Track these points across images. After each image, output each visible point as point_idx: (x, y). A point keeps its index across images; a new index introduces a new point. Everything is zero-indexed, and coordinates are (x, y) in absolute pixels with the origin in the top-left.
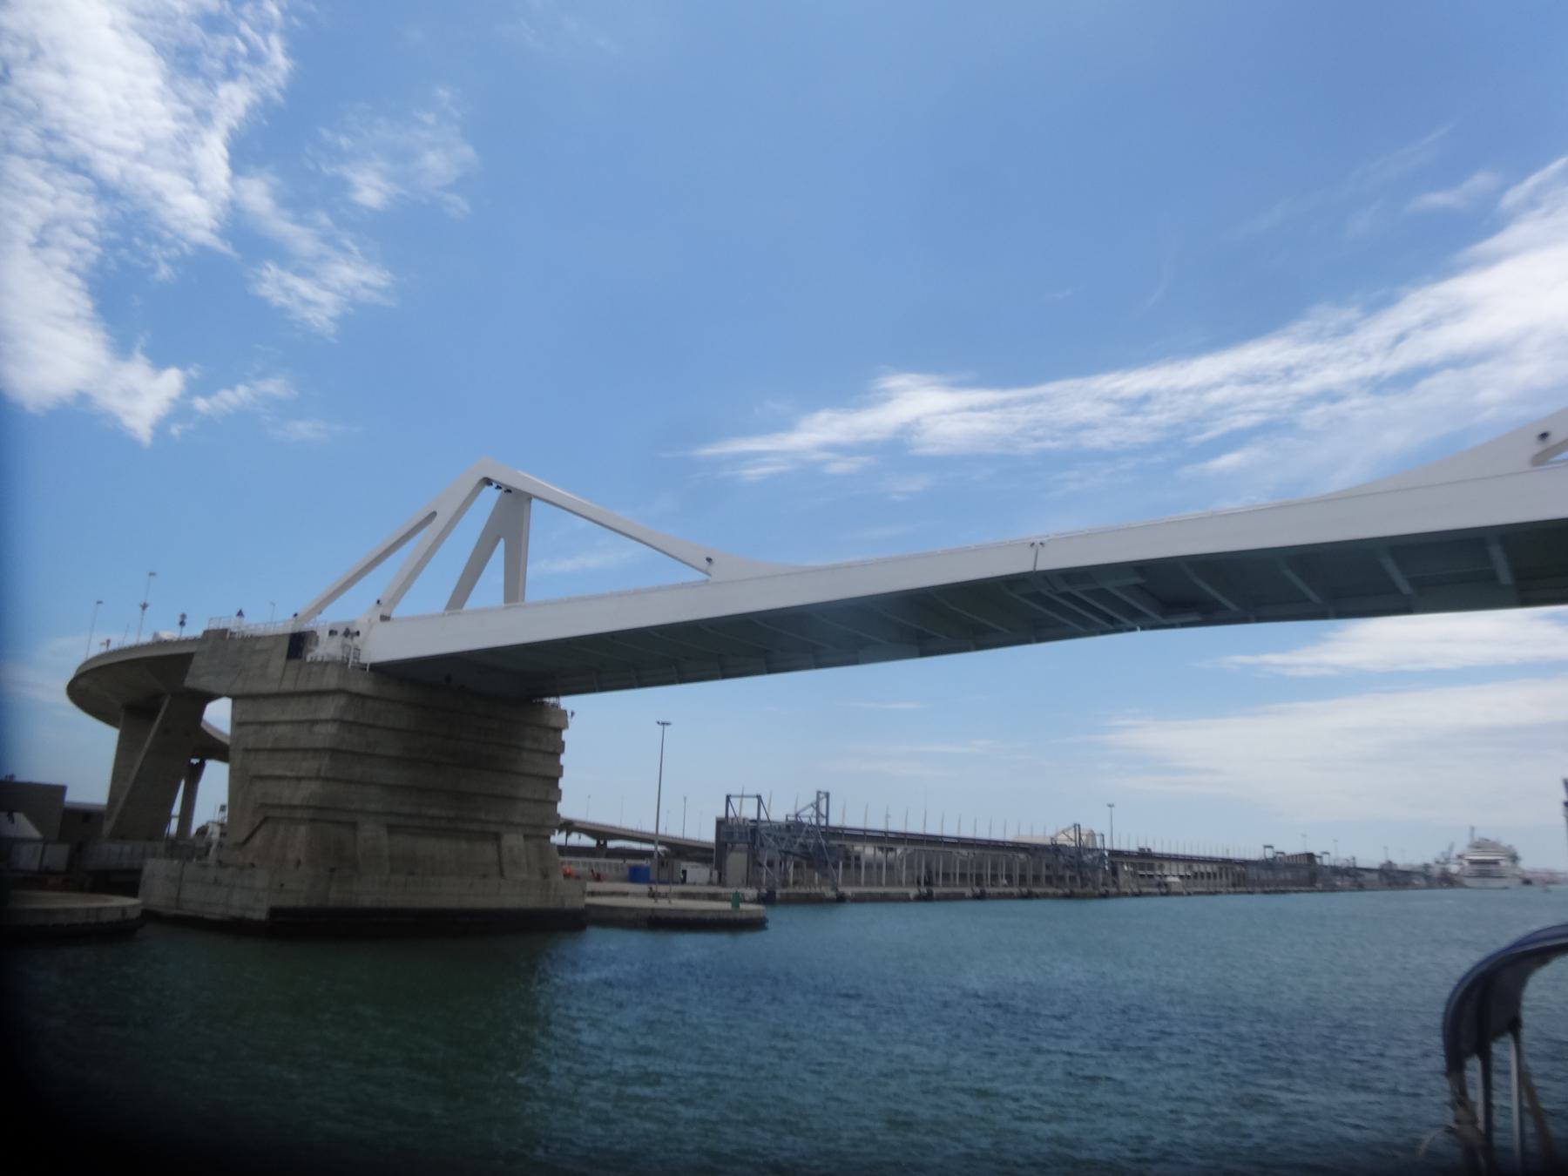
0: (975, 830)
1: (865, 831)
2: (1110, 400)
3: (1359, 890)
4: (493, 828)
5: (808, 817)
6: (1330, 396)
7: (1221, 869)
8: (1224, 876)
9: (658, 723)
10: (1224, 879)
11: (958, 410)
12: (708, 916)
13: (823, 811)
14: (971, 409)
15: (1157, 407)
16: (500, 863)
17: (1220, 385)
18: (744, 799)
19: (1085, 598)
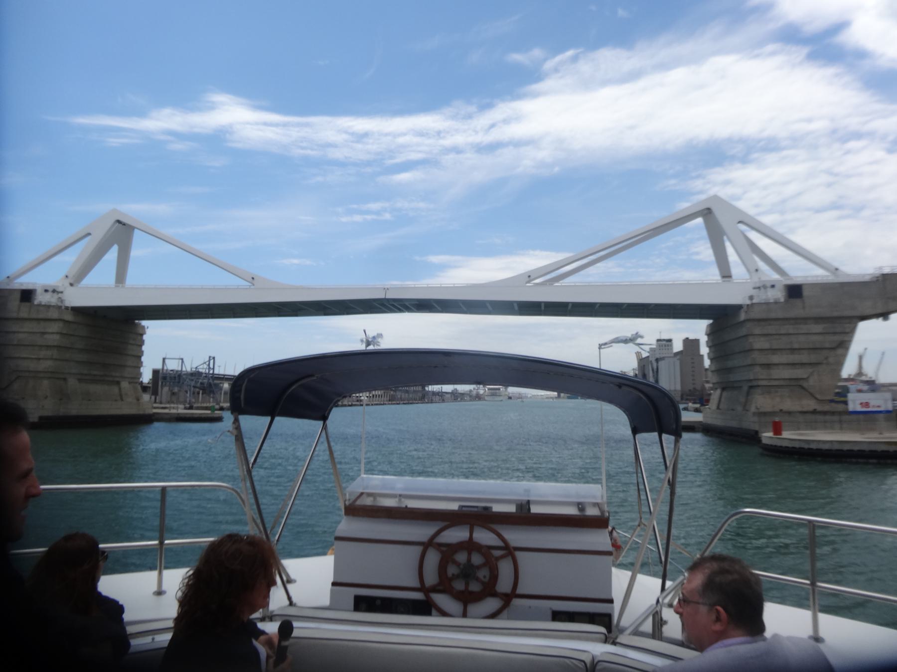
0: (225, 370)
1: (224, 375)
2: (346, 132)
3: (442, 402)
4: (117, 379)
5: (203, 369)
6: (456, 150)
7: (384, 393)
8: (386, 396)
10: (385, 398)
11: (257, 124)
12: (188, 416)
13: (211, 366)
14: (266, 124)
15: (371, 141)
16: (121, 396)
17: (404, 134)
19: (399, 307)
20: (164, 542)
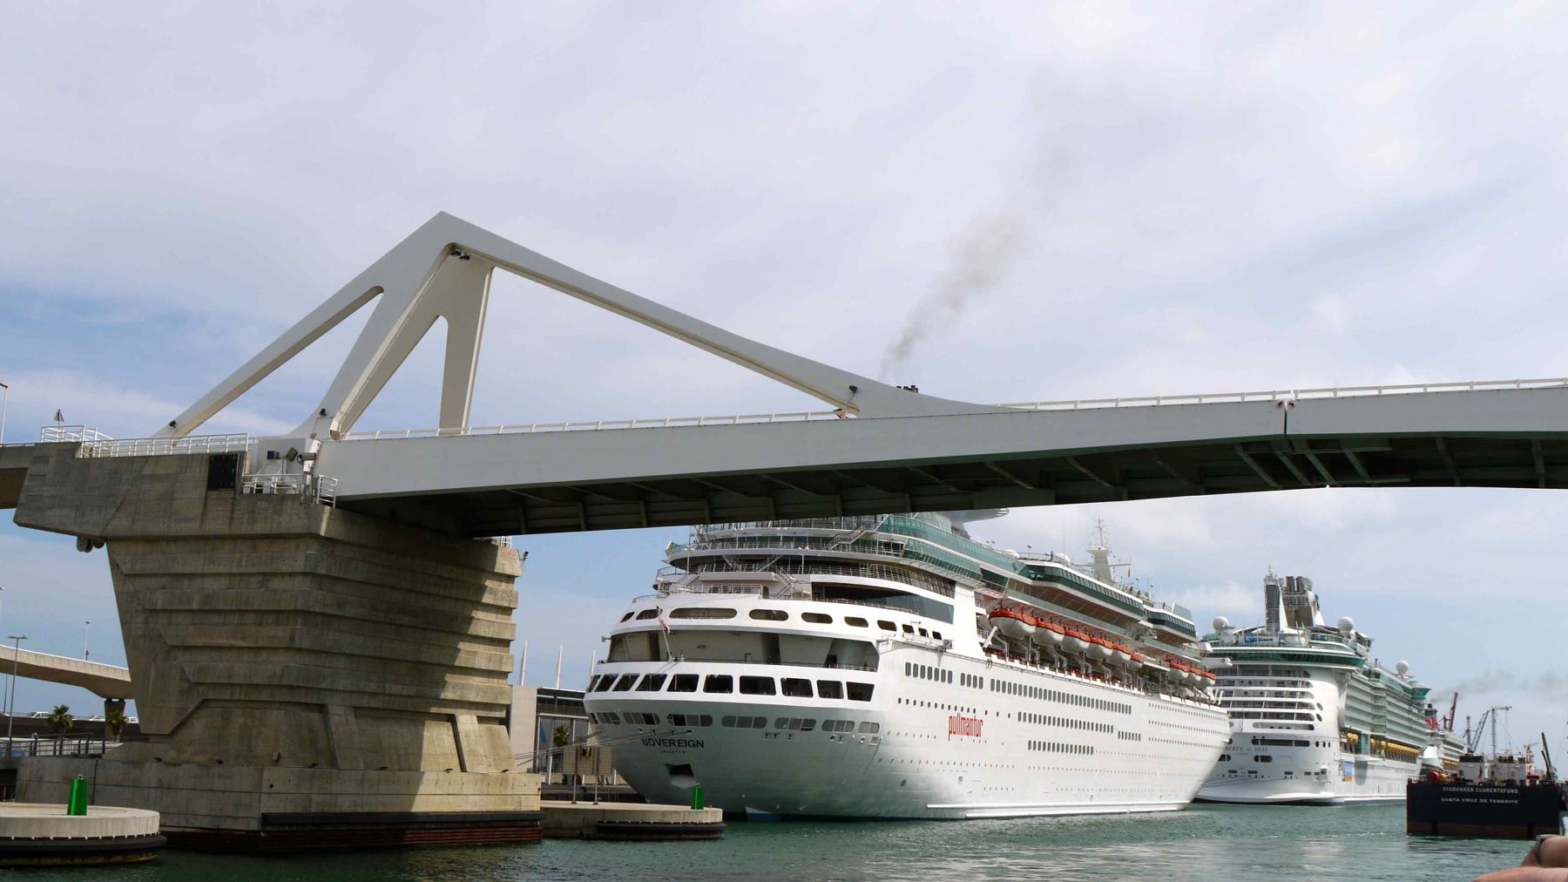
9: (1376, 660)
18: (20, 640)
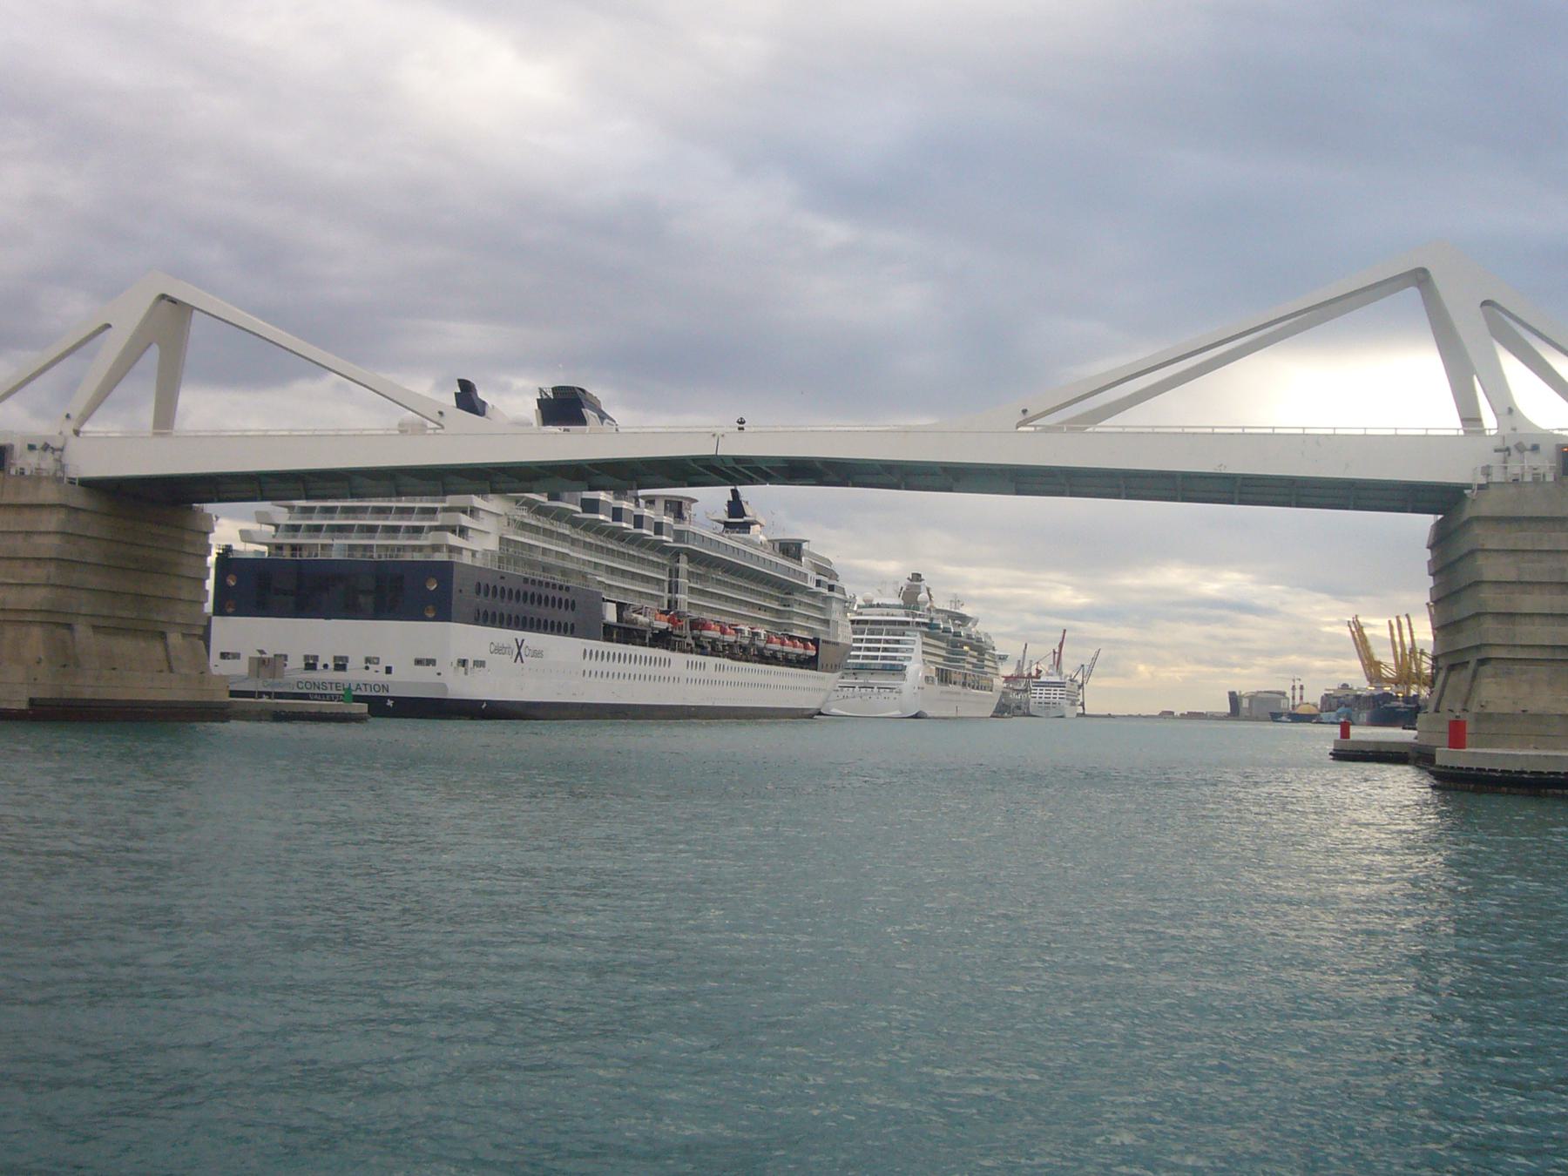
20: (438, 583)
